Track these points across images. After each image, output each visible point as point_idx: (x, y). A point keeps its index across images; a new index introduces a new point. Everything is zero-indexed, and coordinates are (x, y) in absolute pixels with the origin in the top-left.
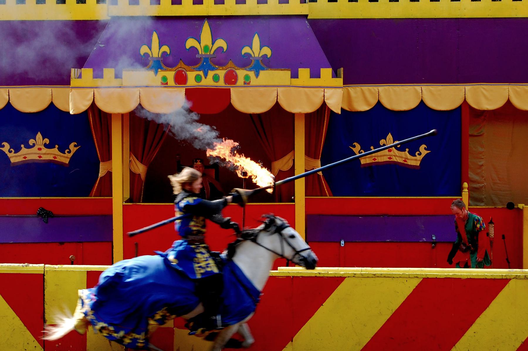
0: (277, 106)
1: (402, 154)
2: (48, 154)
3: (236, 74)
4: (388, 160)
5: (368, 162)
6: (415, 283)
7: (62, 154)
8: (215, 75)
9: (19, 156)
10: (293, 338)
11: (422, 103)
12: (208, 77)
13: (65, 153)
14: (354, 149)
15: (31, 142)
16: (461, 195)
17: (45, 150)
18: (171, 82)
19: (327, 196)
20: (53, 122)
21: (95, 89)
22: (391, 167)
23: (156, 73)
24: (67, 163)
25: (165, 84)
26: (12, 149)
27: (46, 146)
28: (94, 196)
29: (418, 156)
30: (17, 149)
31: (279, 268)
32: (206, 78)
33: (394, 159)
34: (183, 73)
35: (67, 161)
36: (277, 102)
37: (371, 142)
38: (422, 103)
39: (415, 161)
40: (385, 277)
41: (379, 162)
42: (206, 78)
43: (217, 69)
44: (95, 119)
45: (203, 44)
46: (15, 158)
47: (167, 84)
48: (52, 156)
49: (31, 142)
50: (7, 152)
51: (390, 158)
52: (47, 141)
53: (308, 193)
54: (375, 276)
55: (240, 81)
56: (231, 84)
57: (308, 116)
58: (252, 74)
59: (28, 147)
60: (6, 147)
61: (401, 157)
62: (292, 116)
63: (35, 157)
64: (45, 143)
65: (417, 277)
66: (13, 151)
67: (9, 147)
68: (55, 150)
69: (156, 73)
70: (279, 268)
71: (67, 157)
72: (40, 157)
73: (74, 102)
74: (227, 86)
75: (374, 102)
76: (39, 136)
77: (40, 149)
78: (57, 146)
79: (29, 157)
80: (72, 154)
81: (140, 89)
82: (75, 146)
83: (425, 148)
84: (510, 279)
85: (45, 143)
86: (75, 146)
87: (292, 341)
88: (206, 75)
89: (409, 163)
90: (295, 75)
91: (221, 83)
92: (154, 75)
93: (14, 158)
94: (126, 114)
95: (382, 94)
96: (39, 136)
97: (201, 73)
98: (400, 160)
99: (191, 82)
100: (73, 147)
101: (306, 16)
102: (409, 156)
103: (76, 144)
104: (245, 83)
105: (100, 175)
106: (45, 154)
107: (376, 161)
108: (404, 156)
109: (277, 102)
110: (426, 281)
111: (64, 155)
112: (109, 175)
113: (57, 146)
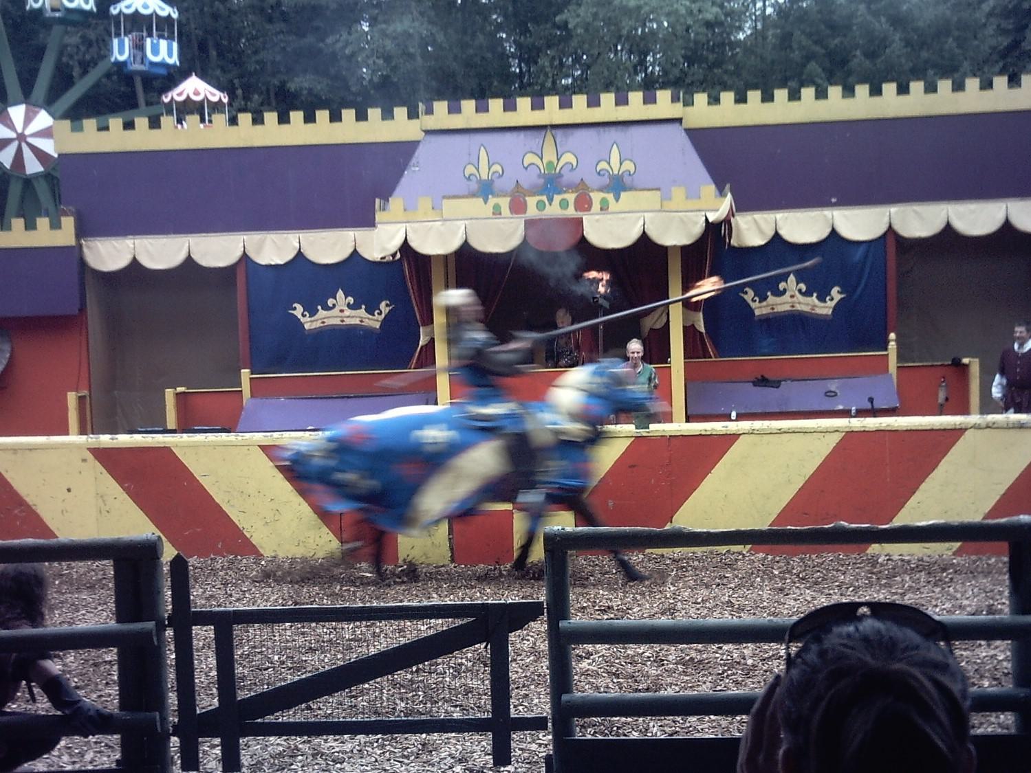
0: (644, 238)
1: (808, 299)
2: (353, 317)
3: (590, 197)
4: (791, 309)
5: (764, 312)
6: (837, 438)
7: (371, 317)
8: (563, 200)
9: (317, 320)
10: (672, 517)
11: (834, 233)
12: (553, 203)
13: (374, 315)
14: (746, 297)
15: (330, 302)
16: (886, 349)
17: (348, 312)
18: (506, 210)
19: (711, 357)
20: (356, 275)
21: (407, 224)
22: (797, 320)
23: (486, 202)
24: (378, 327)
25: (497, 212)
26: (306, 313)
27: (349, 306)
28: (414, 368)
29: (829, 302)
30: (313, 312)
31: (650, 425)
32: (550, 204)
33: (798, 307)
34: (521, 199)
35: (377, 325)
36: (644, 232)
37: (771, 287)
38: (834, 233)
39: (825, 309)
40: (794, 432)
41: (777, 312)
42: (550, 204)
43: (565, 192)
44: (412, 267)
45: (545, 161)
46: (309, 324)
47: (500, 214)
48: (358, 319)
49: (330, 302)
50: (300, 316)
51: (793, 306)
52: (351, 300)
53: (687, 355)
54: (781, 432)
55: (596, 206)
56: (584, 211)
57: (684, 249)
58: (610, 197)
59: (326, 308)
60: (298, 310)
61: (808, 304)
62: (664, 249)
63: (337, 321)
64: (349, 303)
65: (837, 431)
66: (308, 315)
67: (302, 310)
68: (362, 312)
69: (486, 202)
70: (650, 425)
71: (377, 321)
72: (342, 321)
73: (379, 242)
74: (579, 214)
75: (771, 233)
76: (340, 294)
77: (342, 311)
78: (363, 307)
79: (329, 322)
80: (383, 316)
81: (467, 222)
82: (387, 305)
83: (838, 292)
84: (966, 429)
85: (349, 303)
86: (387, 305)
87: (671, 522)
88: (551, 200)
89: (819, 311)
90: (667, 197)
91: (571, 212)
92: (483, 203)
93: (309, 324)
94: (451, 254)
95: (780, 224)
96: (340, 294)
97: (544, 198)
98: (806, 309)
99: (532, 211)
100: (384, 307)
101: (679, 120)
102: (817, 302)
103: (388, 302)
104: (601, 209)
105: (421, 343)
106: (348, 317)
107: (775, 310)
108: (810, 303)
109: (644, 232)
110: (850, 435)
111: (374, 318)
112: (431, 343)
113: (363, 307)
